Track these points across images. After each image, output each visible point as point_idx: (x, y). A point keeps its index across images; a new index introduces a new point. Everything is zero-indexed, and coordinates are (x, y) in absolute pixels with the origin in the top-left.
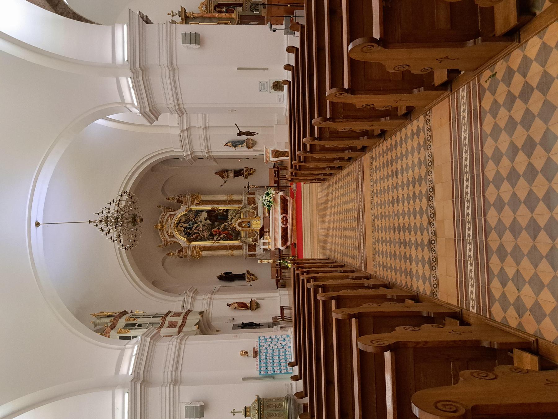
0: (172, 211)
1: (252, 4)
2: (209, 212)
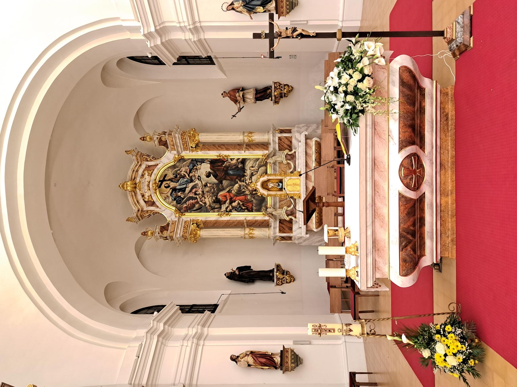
0: (151, 161)
2: (213, 162)
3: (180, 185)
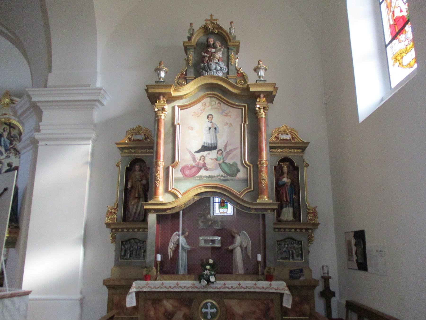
1: (300, 243)
3: (4, 141)
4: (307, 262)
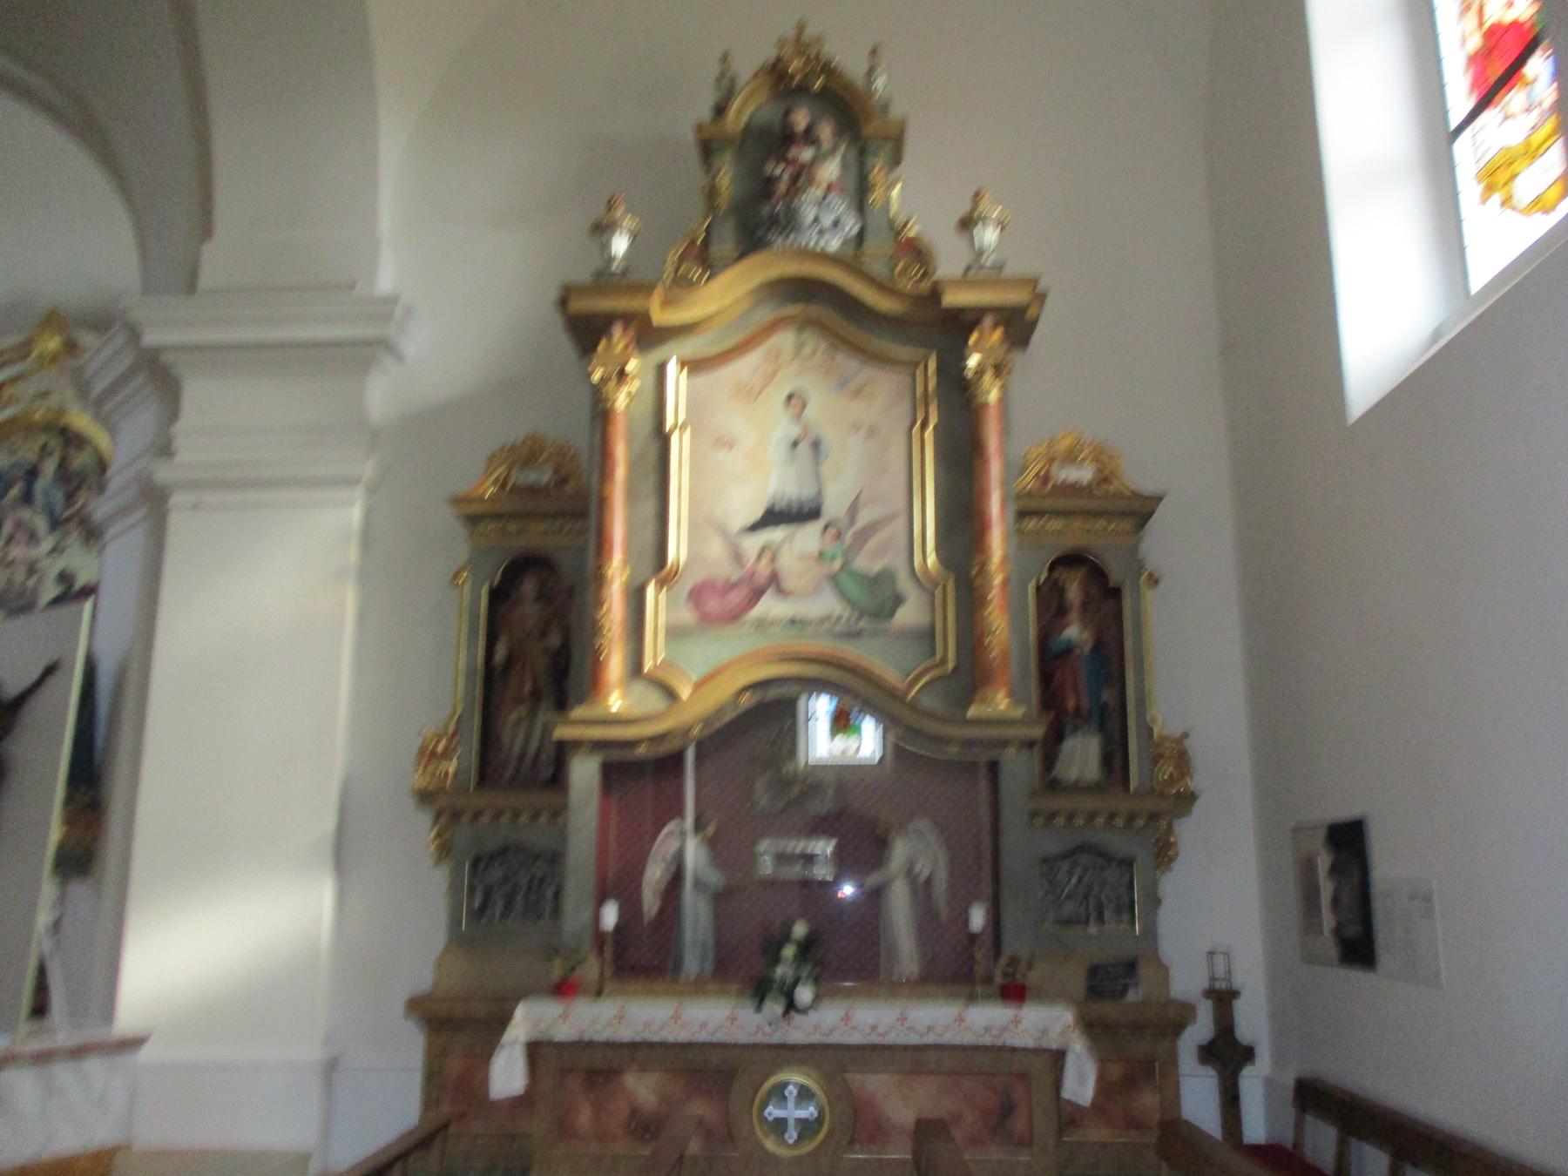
4: (1151, 933)
